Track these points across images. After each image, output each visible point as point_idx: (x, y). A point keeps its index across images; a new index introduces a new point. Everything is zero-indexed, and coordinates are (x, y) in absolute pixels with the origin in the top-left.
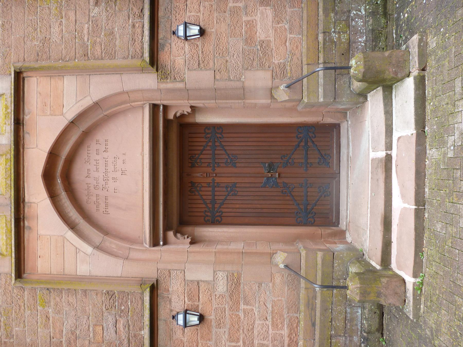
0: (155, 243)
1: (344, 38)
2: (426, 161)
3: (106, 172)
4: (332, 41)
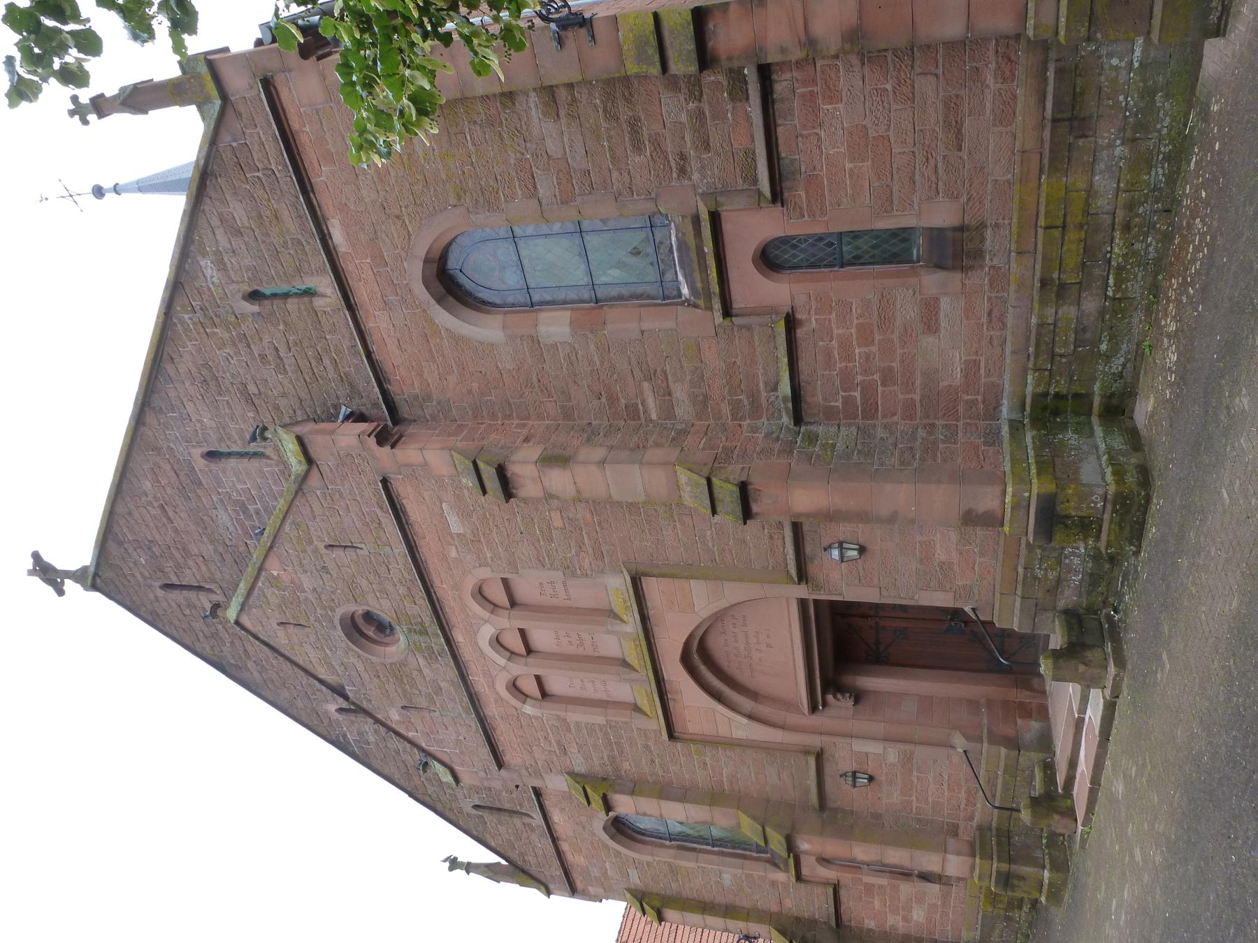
0: (813, 708)
1: (1052, 575)
2: (1159, 658)
3: (747, 643)
4: (1036, 578)
